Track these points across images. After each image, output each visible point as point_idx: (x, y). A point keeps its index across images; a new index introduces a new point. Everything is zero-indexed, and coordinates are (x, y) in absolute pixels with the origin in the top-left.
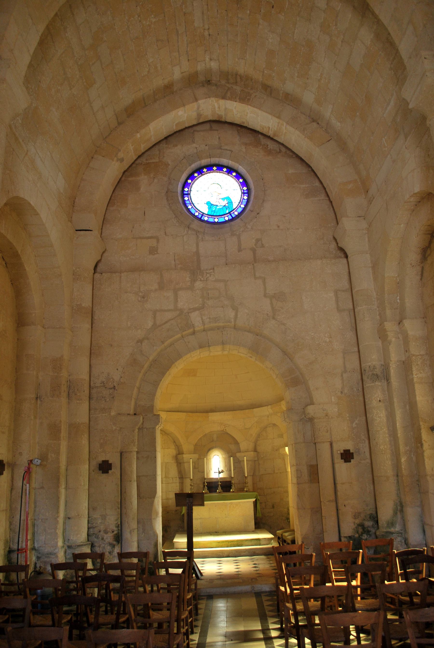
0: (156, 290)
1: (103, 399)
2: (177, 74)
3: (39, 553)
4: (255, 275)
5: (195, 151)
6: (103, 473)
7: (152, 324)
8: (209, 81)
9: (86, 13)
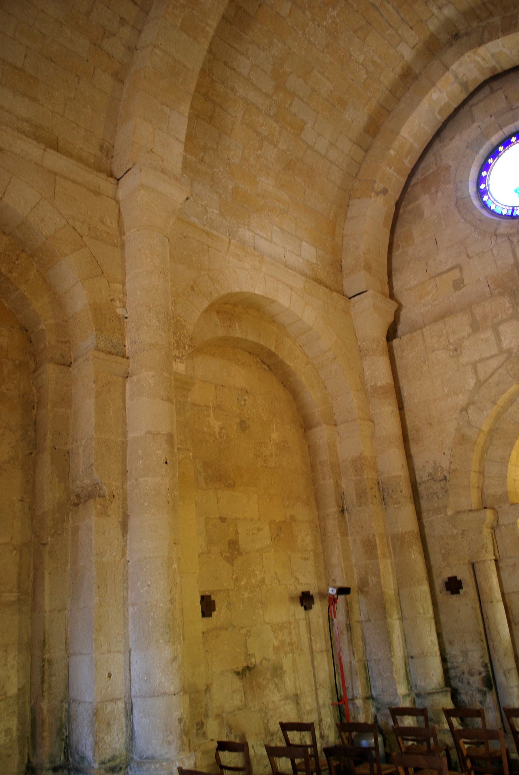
0: (469, 335)
1: (435, 496)
2: (407, 53)
3: (379, 703)
8: (456, 35)
9: (248, 59)
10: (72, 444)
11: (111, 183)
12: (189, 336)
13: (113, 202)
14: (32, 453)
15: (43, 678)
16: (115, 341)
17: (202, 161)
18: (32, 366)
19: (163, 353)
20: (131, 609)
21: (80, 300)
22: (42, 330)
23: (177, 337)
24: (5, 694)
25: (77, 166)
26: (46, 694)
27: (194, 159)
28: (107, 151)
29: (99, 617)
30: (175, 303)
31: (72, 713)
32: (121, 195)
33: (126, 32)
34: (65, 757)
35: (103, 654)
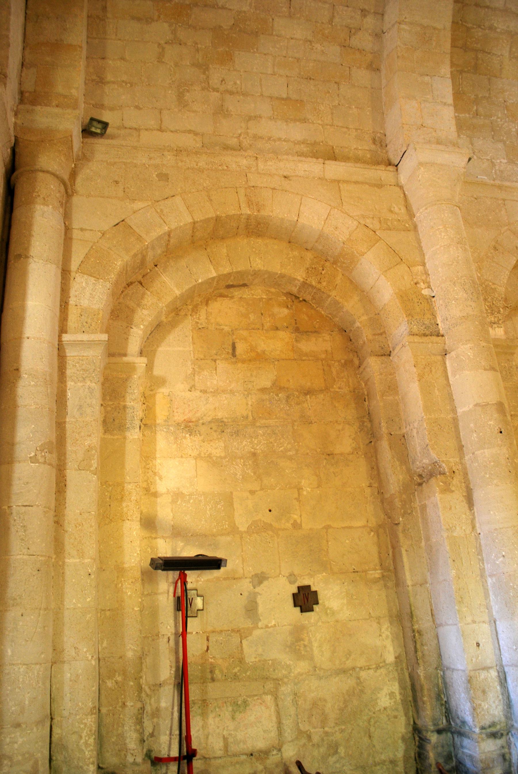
10: (406, 427)
11: (390, 171)
12: (502, 298)
13: (397, 189)
14: (371, 442)
15: (415, 647)
16: (427, 322)
17: (477, 115)
18: (356, 362)
19: (477, 323)
20: (489, 581)
21: (385, 292)
22: (358, 328)
23: (489, 302)
24: (384, 661)
25: (356, 167)
26: (420, 661)
27: (468, 116)
28: (380, 142)
29: (459, 589)
30: (480, 269)
31: (448, 680)
32: (403, 179)
33: (370, 21)
34: (447, 721)
35: (468, 624)
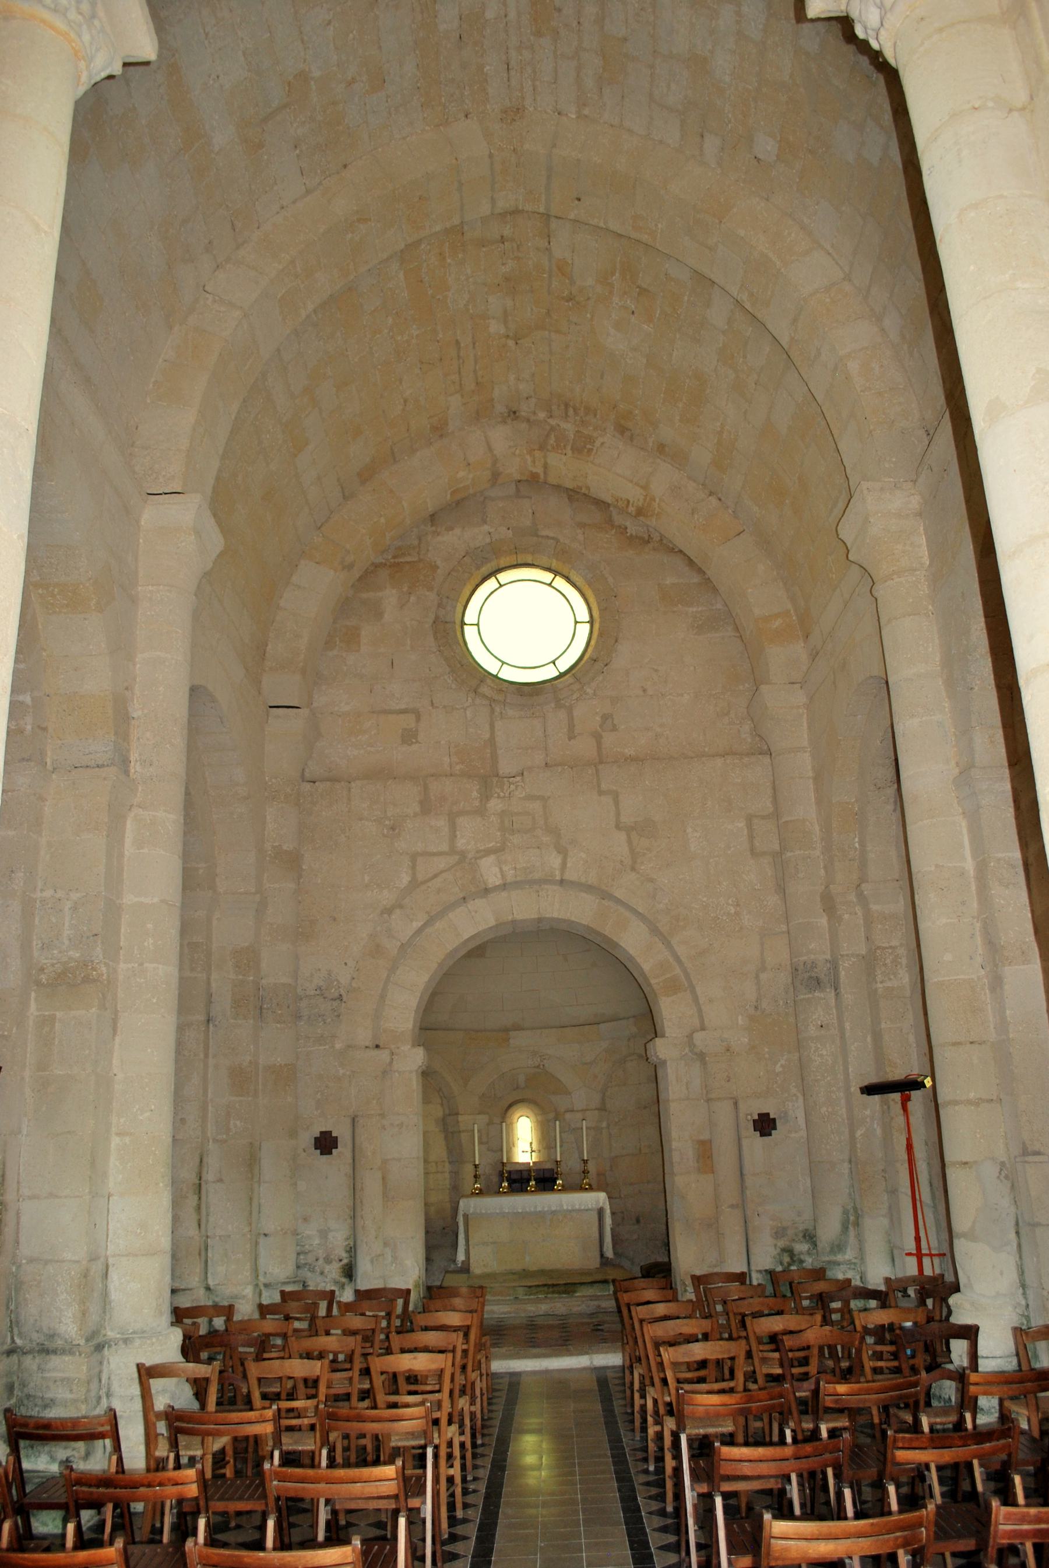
0: (416, 815)
4: (599, 786)
5: (488, 540)
6: (322, 1154)
7: (409, 879)
8: (515, 412)
